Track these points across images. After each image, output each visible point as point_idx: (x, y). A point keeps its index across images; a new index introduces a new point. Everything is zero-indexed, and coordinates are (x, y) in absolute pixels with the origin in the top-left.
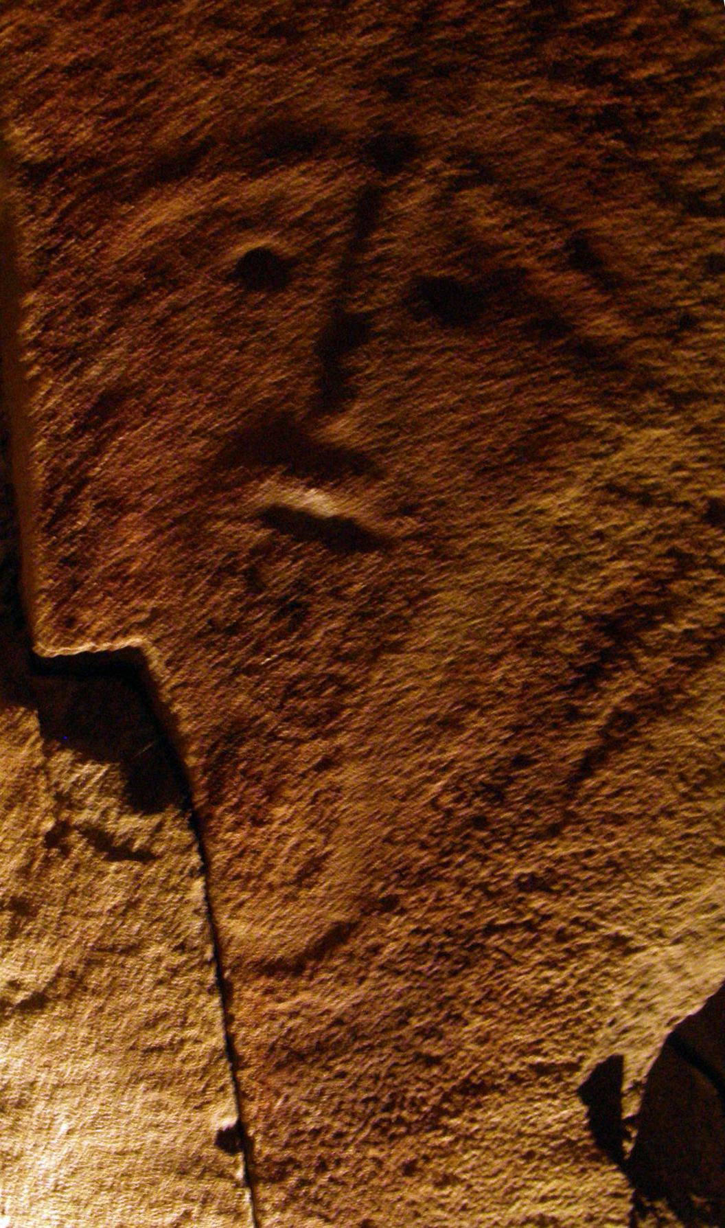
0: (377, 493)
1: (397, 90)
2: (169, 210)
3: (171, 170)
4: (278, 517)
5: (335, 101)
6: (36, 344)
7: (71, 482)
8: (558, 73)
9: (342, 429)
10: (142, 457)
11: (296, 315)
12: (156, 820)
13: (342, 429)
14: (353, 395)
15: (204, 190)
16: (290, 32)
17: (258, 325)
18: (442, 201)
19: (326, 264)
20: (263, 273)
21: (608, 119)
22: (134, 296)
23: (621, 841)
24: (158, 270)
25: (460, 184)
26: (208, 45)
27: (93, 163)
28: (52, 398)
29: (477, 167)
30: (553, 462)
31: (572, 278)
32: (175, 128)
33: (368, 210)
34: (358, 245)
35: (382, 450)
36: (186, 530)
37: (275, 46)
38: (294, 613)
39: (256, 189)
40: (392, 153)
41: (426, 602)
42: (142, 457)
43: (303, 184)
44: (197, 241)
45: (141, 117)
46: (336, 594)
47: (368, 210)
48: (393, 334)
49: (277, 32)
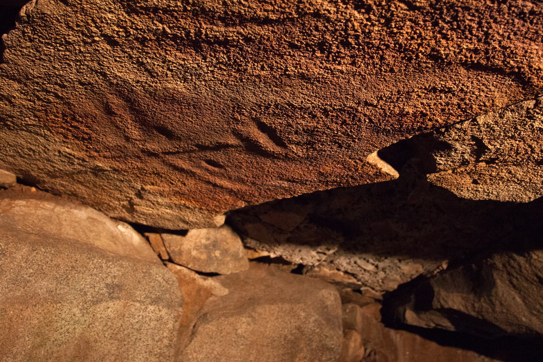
4: (279, 142)
9: (232, 141)
38: (311, 132)
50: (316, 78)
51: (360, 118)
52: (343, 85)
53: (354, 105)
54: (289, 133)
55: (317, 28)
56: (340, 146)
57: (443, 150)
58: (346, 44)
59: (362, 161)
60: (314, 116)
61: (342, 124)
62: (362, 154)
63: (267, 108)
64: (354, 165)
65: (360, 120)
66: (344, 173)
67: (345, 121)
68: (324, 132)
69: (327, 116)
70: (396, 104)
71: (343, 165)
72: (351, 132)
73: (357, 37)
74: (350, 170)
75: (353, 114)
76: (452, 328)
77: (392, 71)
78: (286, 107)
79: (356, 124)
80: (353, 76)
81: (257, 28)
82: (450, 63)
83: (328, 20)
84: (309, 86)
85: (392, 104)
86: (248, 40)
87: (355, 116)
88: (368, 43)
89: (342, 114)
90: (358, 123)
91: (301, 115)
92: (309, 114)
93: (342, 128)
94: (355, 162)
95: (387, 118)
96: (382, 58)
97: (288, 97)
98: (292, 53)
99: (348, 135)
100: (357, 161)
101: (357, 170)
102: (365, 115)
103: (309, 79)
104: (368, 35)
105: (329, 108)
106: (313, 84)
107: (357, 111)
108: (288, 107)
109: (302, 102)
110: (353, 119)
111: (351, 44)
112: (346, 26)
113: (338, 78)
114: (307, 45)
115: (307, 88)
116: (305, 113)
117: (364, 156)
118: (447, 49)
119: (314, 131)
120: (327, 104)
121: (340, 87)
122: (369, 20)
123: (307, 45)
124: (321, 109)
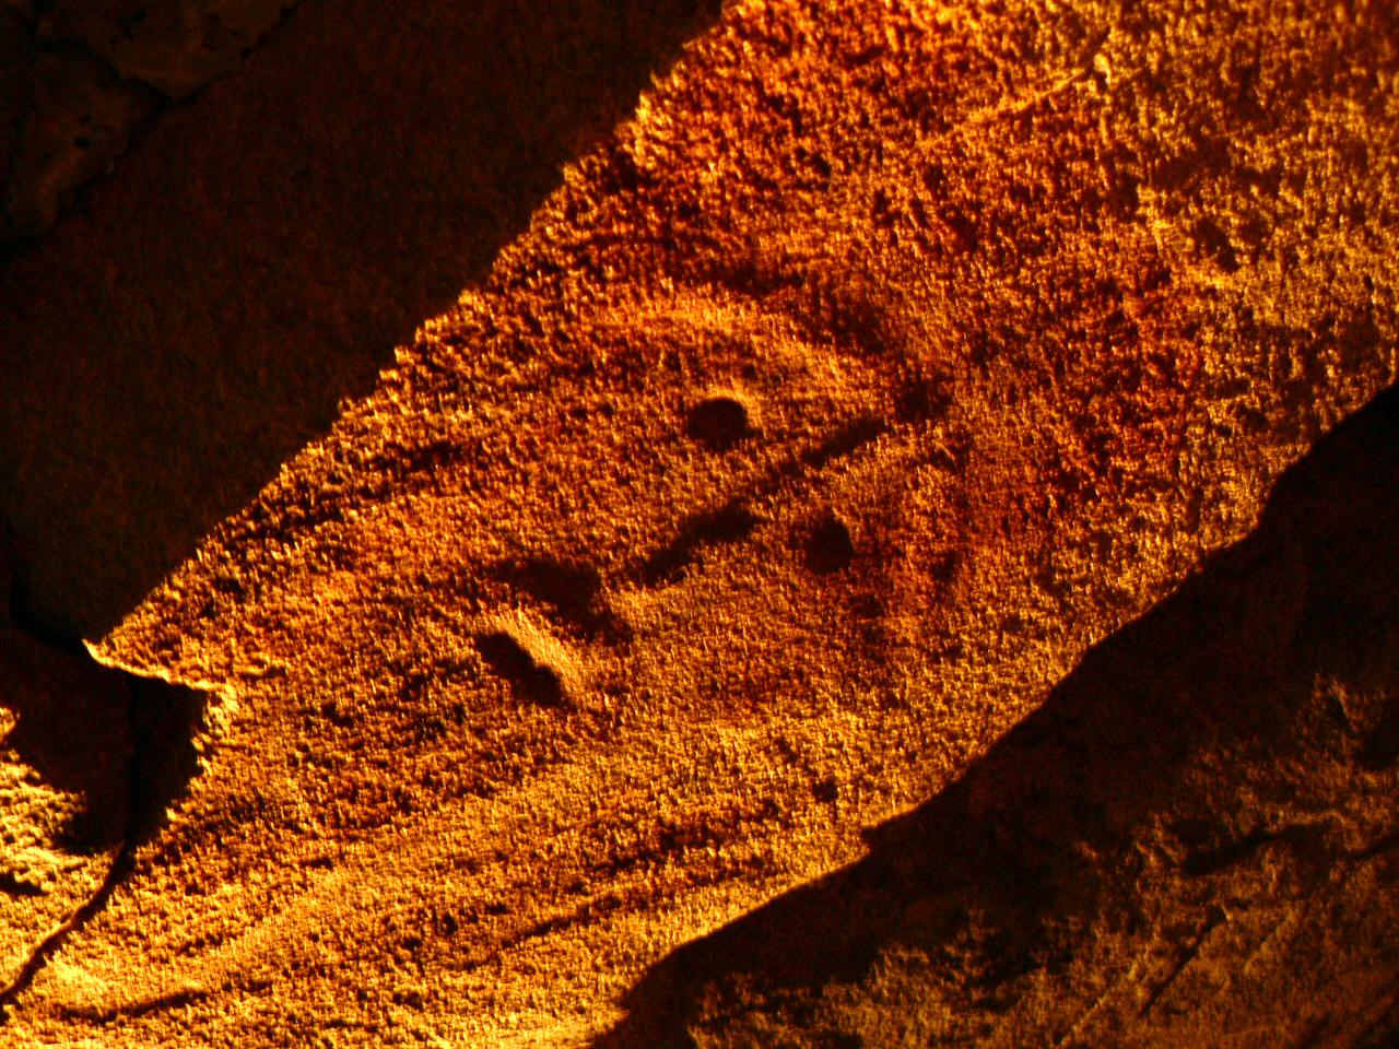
0: (601, 664)
1: (981, 353)
2: (707, 315)
3: (746, 279)
4: (503, 653)
5: (931, 326)
6: (423, 350)
7: (318, 509)
8: (1080, 423)
9: (635, 604)
10: (428, 530)
11: (698, 480)
12: (75, 860)
13: (635, 604)
14: (677, 579)
15: (747, 318)
16: (968, 237)
17: (660, 470)
18: (910, 464)
19: (775, 455)
20: (718, 427)
21: (1068, 481)
22: (582, 371)
23: (519, 987)
24: (630, 363)
25: (937, 459)
26: (902, 193)
27: (689, 211)
28: (384, 417)
29: (960, 456)
30: (764, 707)
31: (925, 580)
32: (795, 242)
33: (855, 434)
34: (816, 459)
35: (645, 634)
36: (395, 613)
37: (947, 237)
38: (424, 731)
39: (793, 350)
40: (920, 400)
41: (122, 665)
42: (428, 530)
43: (833, 376)
44: (689, 360)
45: (778, 206)
46: (479, 732)
47: (855, 434)
48: (760, 549)
49: (959, 224)
50: (446, 873)
51: (323, 823)
52: (390, 878)
53: (351, 848)
54: (478, 707)
55: (466, 950)
56: (329, 710)
57: (64, 823)
58: (410, 943)
59: (245, 677)
60: (425, 782)
61: (356, 787)
62: (257, 704)
63: (539, 760)
64: (257, 650)
65: (320, 818)
66: (272, 600)
67: (352, 801)
68: (389, 746)
69: (397, 793)
70: (265, 886)
71: (288, 630)
72: (325, 778)
73: (399, 961)
74: (257, 620)
75: (346, 830)
76: (85, 642)
77: (314, 938)
78: (496, 780)
79: (324, 805)
80: (376, 903)
81: (561, 912)
82: (227, 988)
83: (450, 967)
84: (455, 849)
85: (274, 883)
86: (577, 888)
87: (336, 825)
88: (377, 958)
89: (366, 814)
90: (322, 810)
91: (458, 772)
92: (439, 783)
93: (350, 780)
94: (260, 663)
95: (264, 847)
96: (342, 948)
97: (496, 810)
98: (498, 896)
99: (327, 764)
100: (254, 670)
101: (240, 633)
102: (315, 837)
103: (458, 865)
104: (383, 970)
105: (400, 817)
106: (451, 856)
107: (338, 839)
108: (492, 783)
109: (463, 809)
110: (336, 815)
111: (404, 947)
112: (421, 970)
113: (405, 888)
114: (474, 919)
115: (458, 843)
116: (451, 782)
117: (248, 700)
118: (247, 1007)
119: (419, 738)
120: (408, 826)
121: (393, 874)
122: (390, 988)
123: (474, 919)
124: (417, 810)
